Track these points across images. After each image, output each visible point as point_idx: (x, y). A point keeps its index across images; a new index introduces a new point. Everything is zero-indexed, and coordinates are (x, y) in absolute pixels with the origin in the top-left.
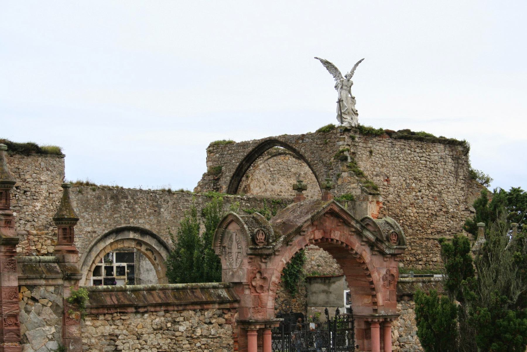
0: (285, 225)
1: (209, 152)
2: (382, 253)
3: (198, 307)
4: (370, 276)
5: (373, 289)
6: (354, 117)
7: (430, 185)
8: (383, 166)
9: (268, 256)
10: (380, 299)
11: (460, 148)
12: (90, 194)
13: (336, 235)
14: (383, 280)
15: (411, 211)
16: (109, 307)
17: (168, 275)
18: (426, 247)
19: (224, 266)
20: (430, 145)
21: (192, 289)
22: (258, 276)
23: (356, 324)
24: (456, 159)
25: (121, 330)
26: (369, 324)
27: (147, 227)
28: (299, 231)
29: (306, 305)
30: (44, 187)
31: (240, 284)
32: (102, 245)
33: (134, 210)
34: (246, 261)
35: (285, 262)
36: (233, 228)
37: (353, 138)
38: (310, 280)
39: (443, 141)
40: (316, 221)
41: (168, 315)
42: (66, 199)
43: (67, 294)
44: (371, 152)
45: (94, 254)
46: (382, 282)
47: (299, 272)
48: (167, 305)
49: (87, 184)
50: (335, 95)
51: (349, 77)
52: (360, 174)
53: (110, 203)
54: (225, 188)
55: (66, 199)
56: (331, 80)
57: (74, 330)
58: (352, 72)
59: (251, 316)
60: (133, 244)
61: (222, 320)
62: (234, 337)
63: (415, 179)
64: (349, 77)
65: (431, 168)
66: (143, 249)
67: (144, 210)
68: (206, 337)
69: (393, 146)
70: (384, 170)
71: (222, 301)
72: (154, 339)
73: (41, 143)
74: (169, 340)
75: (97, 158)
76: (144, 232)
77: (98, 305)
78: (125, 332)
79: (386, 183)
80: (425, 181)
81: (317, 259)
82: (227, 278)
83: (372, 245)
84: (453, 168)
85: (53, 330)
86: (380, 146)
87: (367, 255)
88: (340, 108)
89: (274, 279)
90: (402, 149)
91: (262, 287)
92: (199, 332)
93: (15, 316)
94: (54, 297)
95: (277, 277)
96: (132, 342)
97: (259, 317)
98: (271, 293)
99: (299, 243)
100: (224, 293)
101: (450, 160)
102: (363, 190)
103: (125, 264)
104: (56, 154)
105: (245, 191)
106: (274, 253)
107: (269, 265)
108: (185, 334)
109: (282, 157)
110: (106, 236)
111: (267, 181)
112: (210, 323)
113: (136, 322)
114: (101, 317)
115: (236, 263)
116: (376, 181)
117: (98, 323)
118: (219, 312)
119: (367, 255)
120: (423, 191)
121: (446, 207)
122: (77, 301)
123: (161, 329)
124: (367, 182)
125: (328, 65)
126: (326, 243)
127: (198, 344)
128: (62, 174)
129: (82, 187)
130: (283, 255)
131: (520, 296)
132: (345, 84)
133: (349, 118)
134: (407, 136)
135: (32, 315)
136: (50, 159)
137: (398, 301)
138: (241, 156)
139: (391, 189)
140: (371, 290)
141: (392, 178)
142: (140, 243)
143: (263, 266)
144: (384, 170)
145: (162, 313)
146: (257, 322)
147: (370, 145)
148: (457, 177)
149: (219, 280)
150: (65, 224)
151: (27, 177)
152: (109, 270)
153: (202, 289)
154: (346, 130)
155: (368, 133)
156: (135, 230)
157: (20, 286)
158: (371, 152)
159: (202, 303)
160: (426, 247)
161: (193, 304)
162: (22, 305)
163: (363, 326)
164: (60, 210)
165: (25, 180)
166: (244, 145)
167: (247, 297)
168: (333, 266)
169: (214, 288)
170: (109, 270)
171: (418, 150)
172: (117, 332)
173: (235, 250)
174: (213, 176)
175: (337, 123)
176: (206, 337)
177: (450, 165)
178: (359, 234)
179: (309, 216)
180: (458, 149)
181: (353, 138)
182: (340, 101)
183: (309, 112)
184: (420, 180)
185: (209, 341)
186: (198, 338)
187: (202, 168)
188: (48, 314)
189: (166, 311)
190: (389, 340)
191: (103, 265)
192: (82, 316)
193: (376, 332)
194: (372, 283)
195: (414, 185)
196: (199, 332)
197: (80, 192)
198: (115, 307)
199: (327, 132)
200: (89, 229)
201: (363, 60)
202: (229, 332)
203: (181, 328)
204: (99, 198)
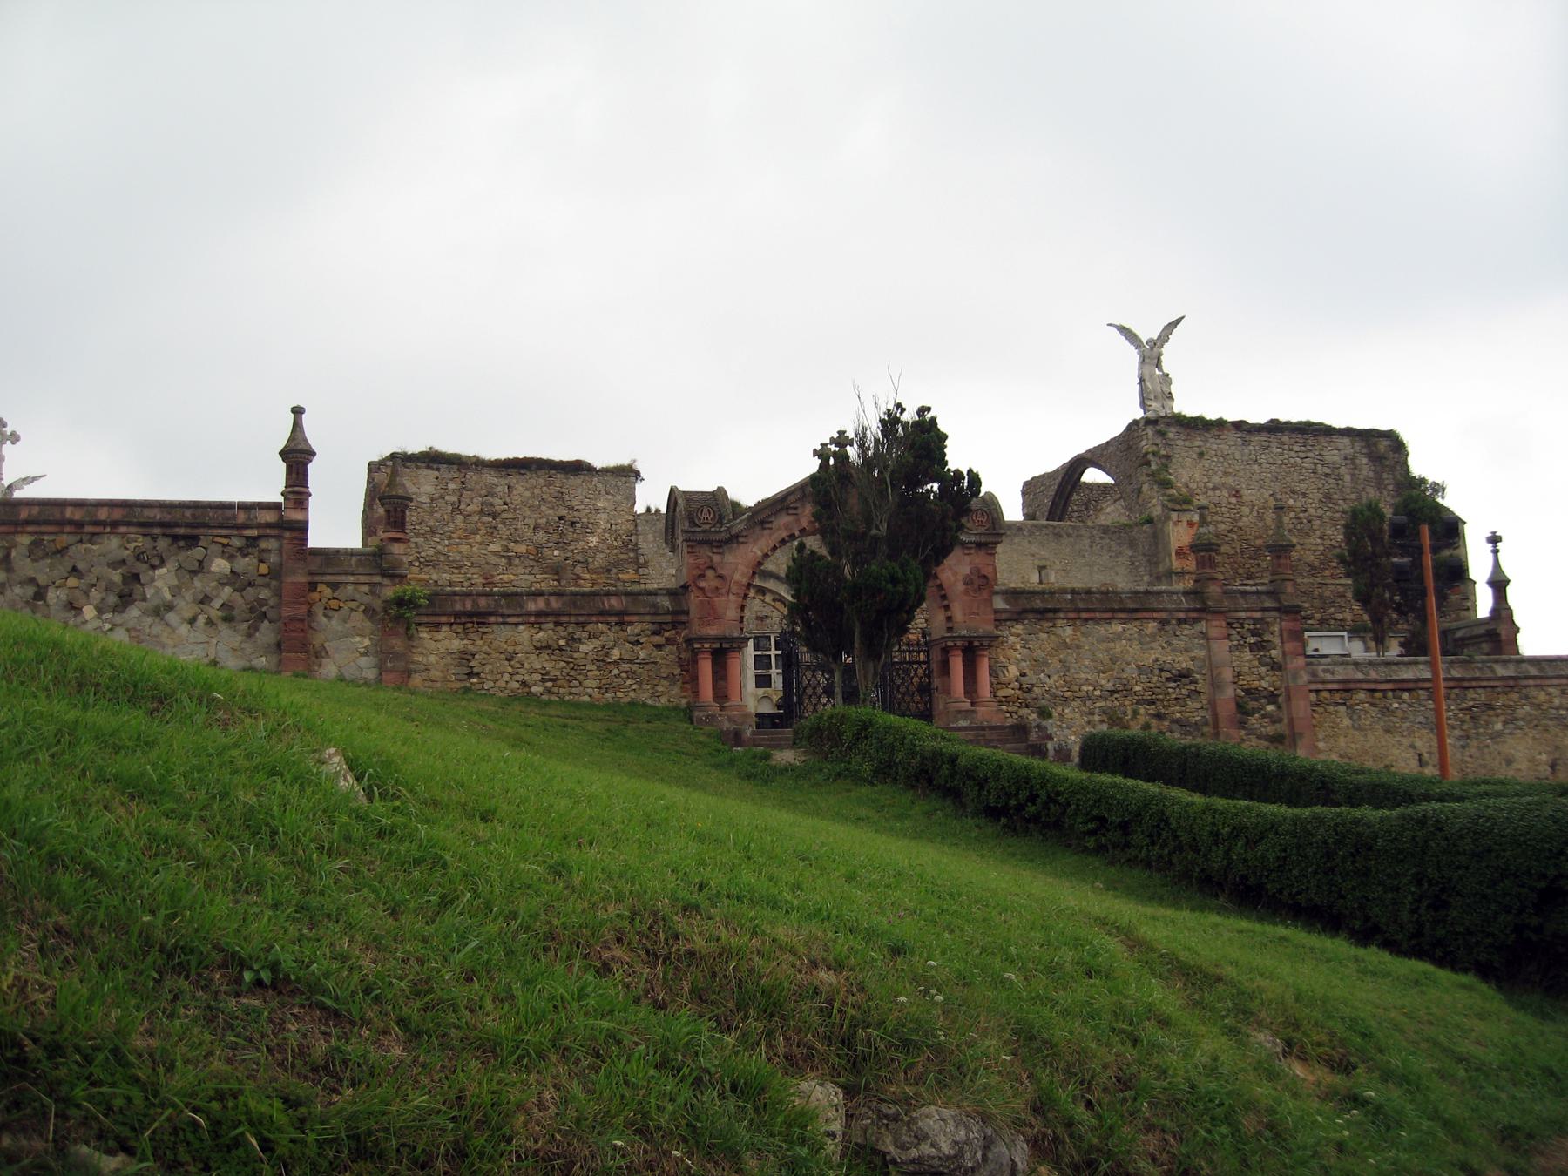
1: (1024, 493)
3: (613, 619)
5: (944, 597)
8: (1226, 474)
10: (958, 613)
14: (965, 583)
18: (1321, 596)
20: (1322, 439)
26: (946, 651)
30: (602, 516)
35: (760, 553)
37: (1162, 434)
39: (1349, 432)
41: (560, 628)
46: (961, 587)
59: (698, 629)
61: (658, 639)
63: (1293, 492)
65: (1326, 475)
68: (630, 661)
74: (563, 664)
78: (485, 648)
79: (1233, 500)
80: (1315, 495)
84: (1371, 474)
85: (367, 642)
89: (737, 577)
90: (1264, 448)
92: (616, 654)
94: (368, 599)
95: (743, 575)
97: (712, 631)
98: (732, 597)
99: (787, 527)
101: (1365, 461)
108: (591, 656)
112: (638, 643)
113: (502, 635)
114: (444, 628)
117: (440, 636)
118: (655, 627)
120: (1312, 511)
123: (548, 647)
127: (616, 672)
130: (755, 542)
134: (1275, 427)
139: (1246, 510)
141: (1245, 492)
143: (716, 558)
144: (1230, 481)
145: (551, 625)
147: (1197, 443)
151: (575, 503)
155: (1198, 425)
158: (1201, 455)
160: (1321, 596)
165: (571, 508)
166: (1057, 471)
171: (1296, 448)
176: (630, 661)
181: (1162, 434)
184: (1304, 495)
185: (634, 667)
186: (615, 662)
189: (557, 624)
193: (957, 664)
195: (1291, 502)
196: (616, 654)
198: (470, 615)
201: (1178, 321)
202: (671, 658)
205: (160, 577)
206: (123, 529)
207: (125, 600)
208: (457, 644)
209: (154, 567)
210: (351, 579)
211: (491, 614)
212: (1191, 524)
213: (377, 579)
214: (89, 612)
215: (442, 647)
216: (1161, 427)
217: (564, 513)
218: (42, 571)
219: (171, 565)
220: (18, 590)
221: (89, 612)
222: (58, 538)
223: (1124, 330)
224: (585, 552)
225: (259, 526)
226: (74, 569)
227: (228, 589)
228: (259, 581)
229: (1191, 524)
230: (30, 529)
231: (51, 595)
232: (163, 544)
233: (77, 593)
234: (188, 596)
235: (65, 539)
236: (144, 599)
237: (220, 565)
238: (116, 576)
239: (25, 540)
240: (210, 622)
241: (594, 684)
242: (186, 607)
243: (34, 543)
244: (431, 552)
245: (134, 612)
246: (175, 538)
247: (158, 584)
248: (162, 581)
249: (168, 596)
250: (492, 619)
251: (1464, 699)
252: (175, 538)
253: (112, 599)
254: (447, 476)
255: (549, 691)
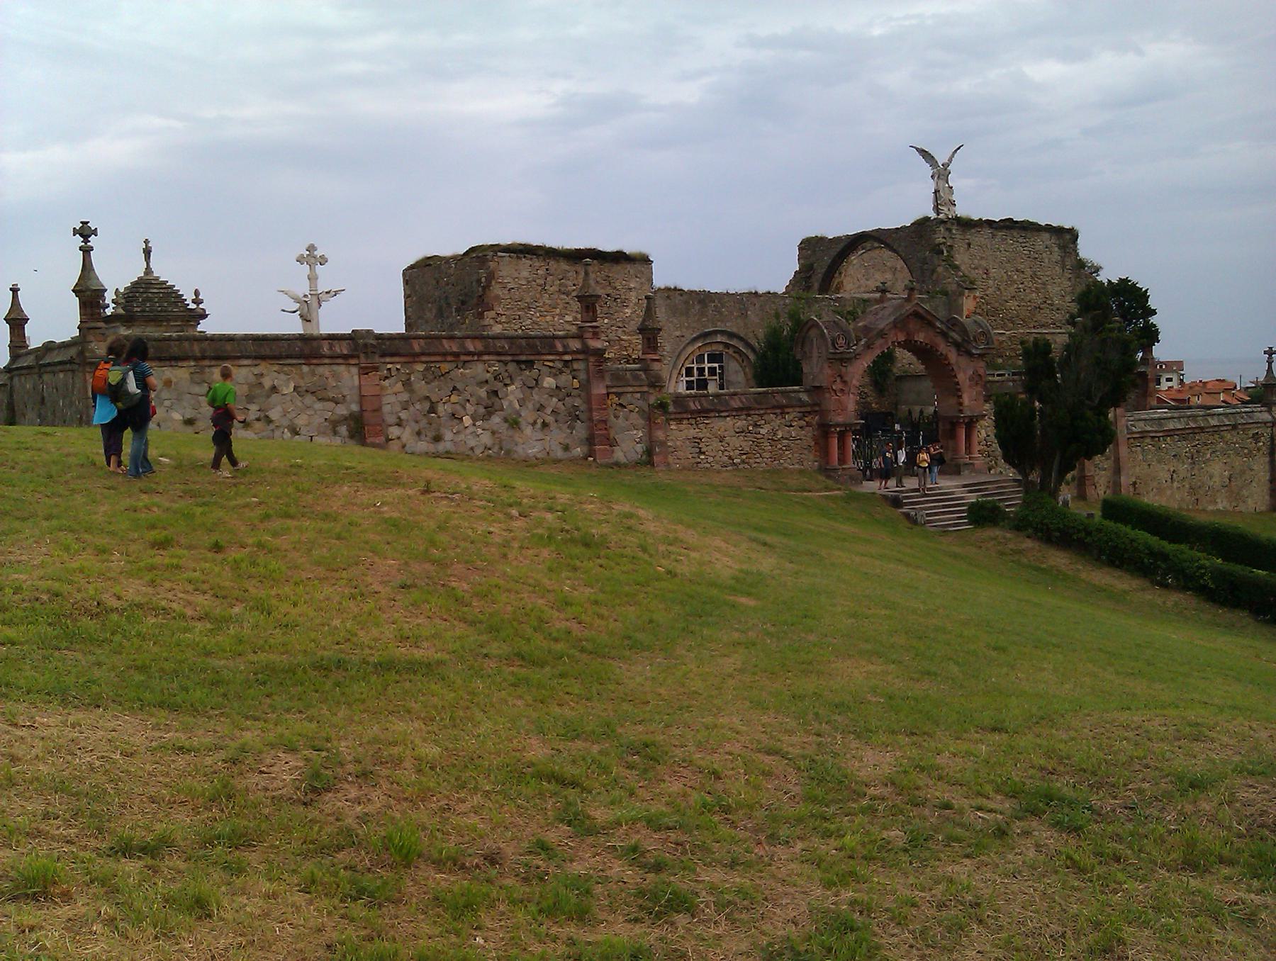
0: (866, 329)
2: (971, 355)
3: (778, 411)
4: (955, 376)
5: (959, 390)
6: (952, 208)
7: (1034, 276)
8: (982, 258)
9: (849, 360)
10: (966, 400)
11: (1068, 237)
12: (678, 299)
13: (920, 337)
15: (1013, 304)
16: (692, 412)
17: (756, 376)
19: (805, 370)
21: (773, 392)
22: (838, 380)
23: (940, 424)
24: (1063, 248)
25: (704, 433)
27: (735, 330)
28: (882, 334)
29: (896, 404)
30: (633, 294)
31: (820, 387)
32: (690, 349)
33: (720, 313)
34: (826, 365)
36: (813, 333)
37: (949, 230)
38: (899, 378)
39: (1049, 229)
40: (899, 324)
42: (649, 311)
43: (652, 400)
44: (969, 245)
45: (683, 358)
47: (890, 370)
48: (749, 409)
49: (675, 289)
50: (931, 185)
51: (946, 166)
52: (957, 268)
53: (697, 307)
54: (816, 286)
55: (649, 311)
56: (929, 170)
57: (660, 435)
58: (950, 160)
60: (721, 348)
62: (815, 438)
64: (946, 166)
66: (731, 351)
67: (731, 313)
69: (994, 236)
70: (983, 263)
71: (803, 404)
72: (737, 442)
73: (628, 250)
75: (685, 262)
76: (732, 335)
77: (681, 410)
80: (1029, 272)
81: (905, 359)
82: (808, 381)
83: (957, 345)
86: (981, 238)
87: (953, 356)
88: (936, 199)
89: (854, 382)
91: (842, 390)
93: (605, 422)
96: (716, 444)
97: (840, 419)
100: (804, 397)
102: (959, 285)
103: (716, 365)
104: (644, 260)
105: (838, 290)
106: (857, 356)
107: (850, 369)
109: (877, 252)
110: (695, 340)
111: (857, 280)
115: (816, 369)
116: (973, 274)
119: (953, 356)
121: (1051, 299)
122: (662, 406)
124: (964, 276)
125: (924, 154)
126: (909, 345)
128: (651, 280)
129: (672, 293)
131: (1101, 398)
132: (941, 173)
133: (945, 209)
134: (1009, 224)
135: (620, 421)
136: (638, 266)
137: (986, 401)
138: (833, 253)
140: (956, 391)
142: (727, 346)
144: (983, 263)
146: (838, 425)
148: (1063, 267)
149: (799, 383)
150: (650, 335)
152: (701, 371)
153: (783, 392)
154: (942, 222)
155: (966, 224)
156: (723, 333)
157: (608, 394)
159: (782, 407)
161: (774, 407)
162: (611, 411)
163: (948, 427)
164: (644, 320)
166: (837, 240)
167: (830, 401)
168: (919, 367)
169: (795, 391)
170: (701, 371)
172: (701, 435)
173: (815, 354)
174: (803, 278)
175: (933, 215)
177: (1056, 255)
178: (944, 335)
179: (892, 318)
180: (1066, 237)
181: (949, 230)
182: (936, 192)
183: (905, 204)
187: (792, 265)
188: (636, 419)
190: (975, 440)
191: (695, 366)
192: (668, 420)
193: (962, 433)
194: (958, 384)
197: (668, 297)
198: (699, 412)
199: (923, 223)
200: (678, 333)
203: (762, 431)
204: (686, 302)
205: (512, 392)
206: (486, 358)
207: (490, 411)
208: (693, 432)
209: (506, 385)
210: (631, 389)
211: (712, 411)
212: (975, 298)
213: (646, 389)
214: (467, 420)
215: (683, 434)
216: (949, 225)
217: (610, 291)
218: (435, 390)
219: (518, 383)
220: (418, 406)
221: (467, 420)
222: (442, 365)
223: (923, 153)
224: (623, 321)
225: (573, 352)
226: (455, 388)
227: (555, 400)
228: (575, 393)
229: (975, 298)
230: (424, 359)
231: (440, 408)
232: (512, 367)
233: (458, 407)
234: (530, 406)
235: (445, 367)
236: (502, 410)
237: (549, 382)
238: (482, 392)
239: (420, 367)
240: (545, 425)
241: (767, 455)
242: (527, 415)
243: (426, 369)
244: (529, 322)
245: (496, 419)
246: (518, 362)
247: (511, 397)
248: (513, 392)
249: (517, 406)
250: (712, 414)
251: (1194, 439)
252: (518, 362)
253: (482, 410)
254: (537, 264)
255: (743, 461)
